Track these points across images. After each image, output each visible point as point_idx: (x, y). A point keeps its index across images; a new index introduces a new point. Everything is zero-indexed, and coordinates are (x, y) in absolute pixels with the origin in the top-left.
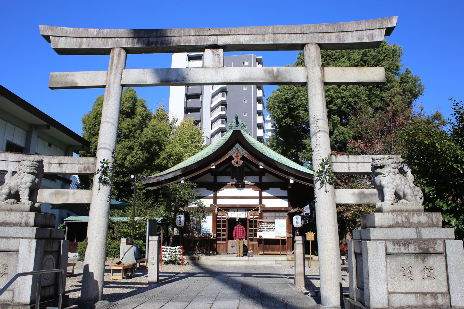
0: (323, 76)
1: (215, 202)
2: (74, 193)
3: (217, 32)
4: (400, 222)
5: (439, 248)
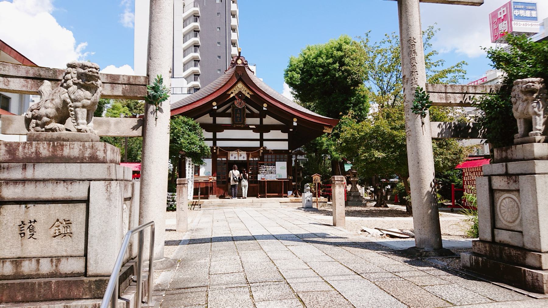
1: (215, 144)
2: (117, 123)
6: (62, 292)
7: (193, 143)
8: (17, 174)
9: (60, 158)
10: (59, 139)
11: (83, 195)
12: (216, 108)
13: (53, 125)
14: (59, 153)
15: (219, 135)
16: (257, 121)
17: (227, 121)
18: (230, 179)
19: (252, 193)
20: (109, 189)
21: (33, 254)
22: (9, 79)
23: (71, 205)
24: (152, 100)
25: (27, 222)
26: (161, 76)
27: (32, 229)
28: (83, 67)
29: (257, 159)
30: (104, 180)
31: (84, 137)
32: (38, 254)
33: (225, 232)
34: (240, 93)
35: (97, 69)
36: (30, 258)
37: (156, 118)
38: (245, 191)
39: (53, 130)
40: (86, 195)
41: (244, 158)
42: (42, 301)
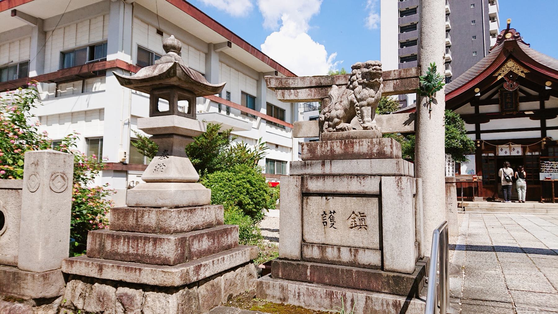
1: (478, 137)
2: (388, 120)
6: (362, 281)
7: (454, 138)
8: (317, 170)
9: (351, 154)
10: (348, 137)
11: (376, 190)
12: (479, 94)
13: (343, 125)
14: (350, 150)
15: (484, 126)
16: (536, 105)
18: (500, 178)
19: (530, 197)
20: (399, 185)
21: (334, 242)
22: (298, 90)
23: (364, 198)
24: (425, 91)
25: (328, 212)
26: (434, 64)
27: (332, 219)
28: (368, 66)
29: (537, 153)
30: (394, 175)
31: (371, 134)
32: (339, 243)
33: (509, 241)
34: (511, 72)
35: (380, 66)
36: (332, 246)
37: (430, 111)
38: (522, 194)
39: (342, 129)
40: (378, 189)
41: (518, 152)
42: (345, 288)
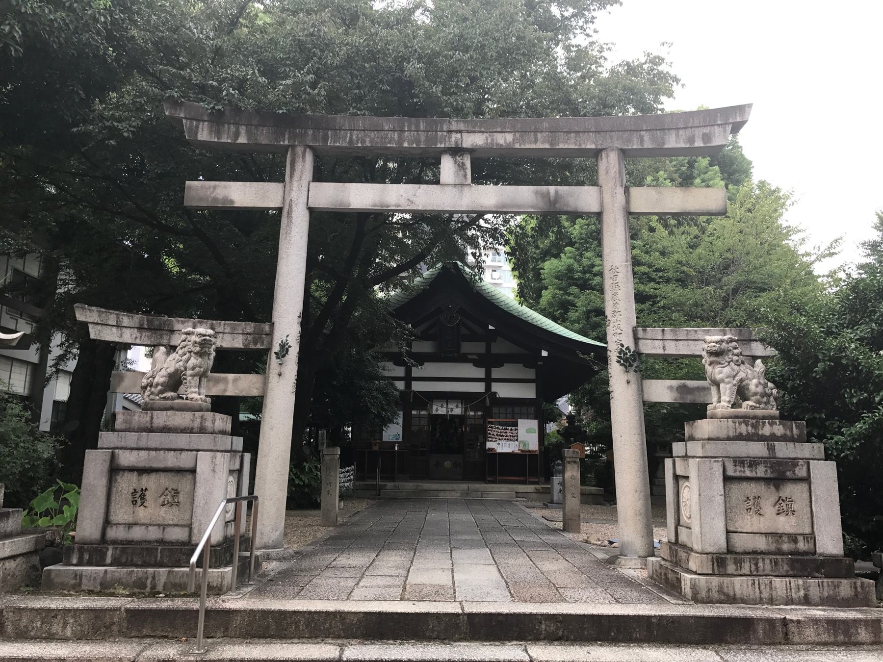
0: (628, 201)
2: (235, 380)
3: (462, 126)
4: (745, 433)
5: (801, 472)
16: (478, 348)
17: (425, 347)
25: (139, 490)
27: (143, 497)
